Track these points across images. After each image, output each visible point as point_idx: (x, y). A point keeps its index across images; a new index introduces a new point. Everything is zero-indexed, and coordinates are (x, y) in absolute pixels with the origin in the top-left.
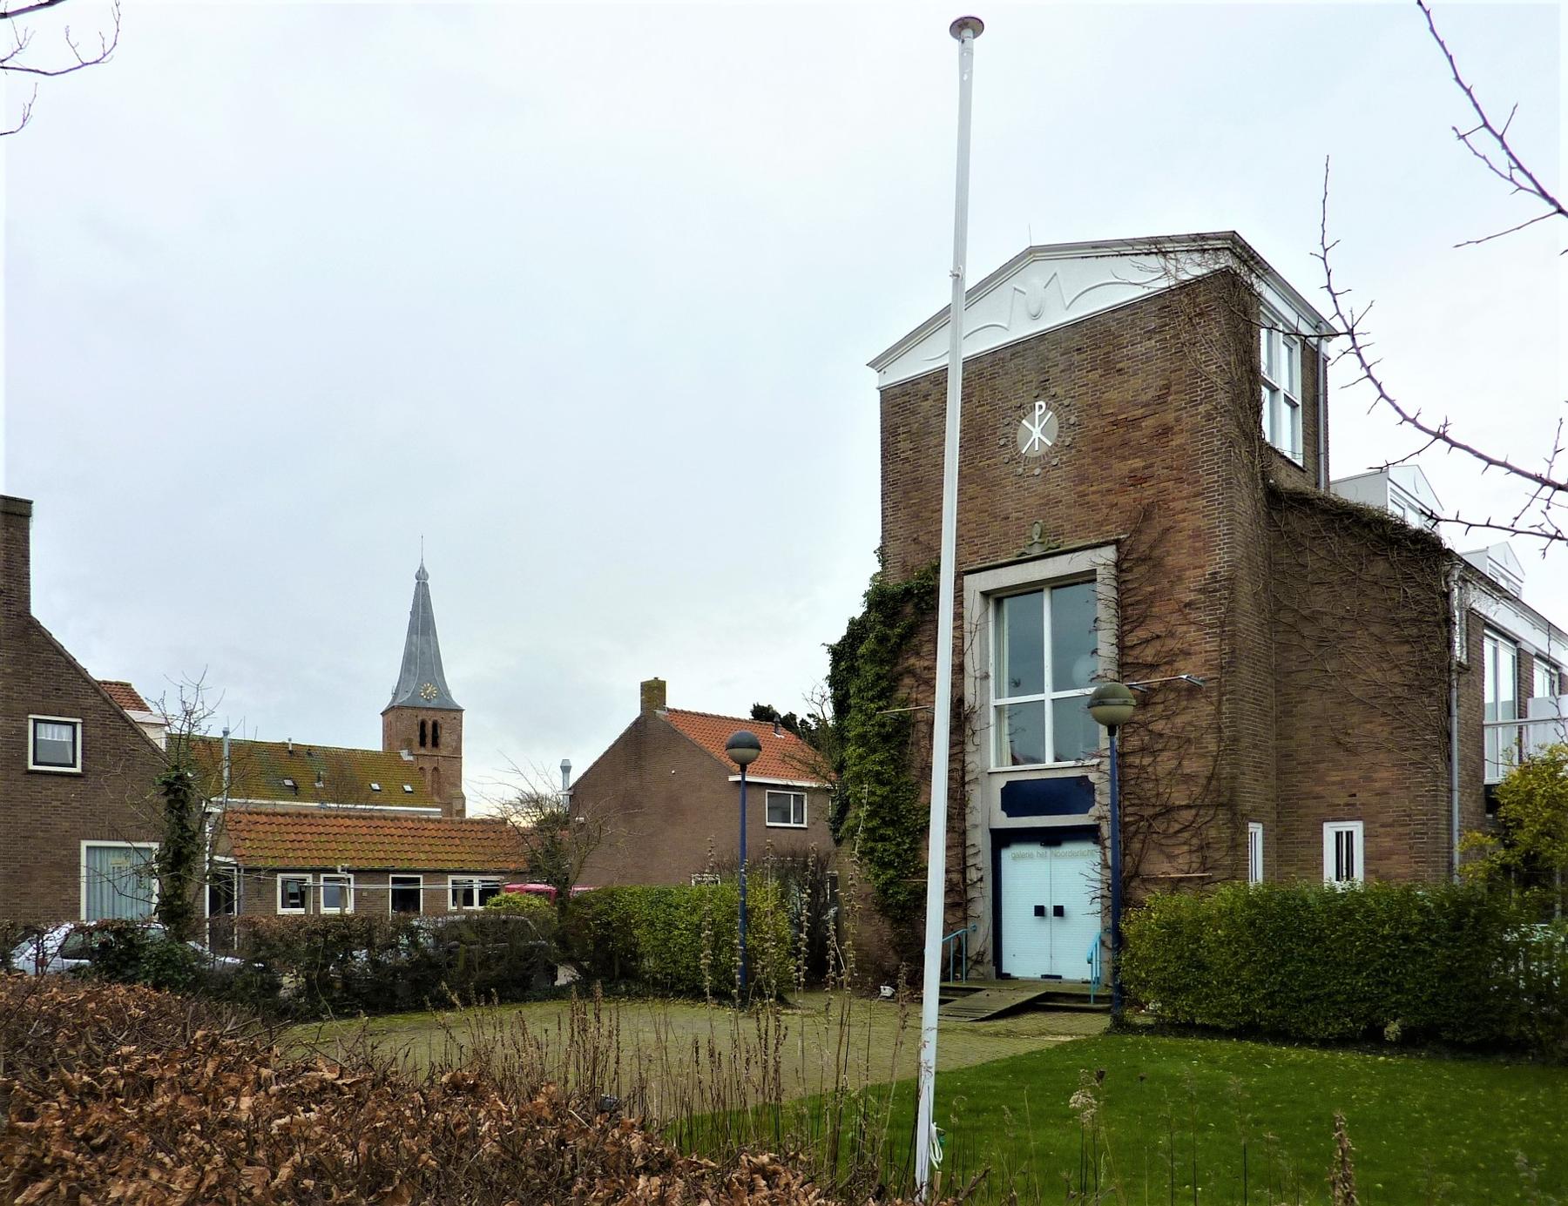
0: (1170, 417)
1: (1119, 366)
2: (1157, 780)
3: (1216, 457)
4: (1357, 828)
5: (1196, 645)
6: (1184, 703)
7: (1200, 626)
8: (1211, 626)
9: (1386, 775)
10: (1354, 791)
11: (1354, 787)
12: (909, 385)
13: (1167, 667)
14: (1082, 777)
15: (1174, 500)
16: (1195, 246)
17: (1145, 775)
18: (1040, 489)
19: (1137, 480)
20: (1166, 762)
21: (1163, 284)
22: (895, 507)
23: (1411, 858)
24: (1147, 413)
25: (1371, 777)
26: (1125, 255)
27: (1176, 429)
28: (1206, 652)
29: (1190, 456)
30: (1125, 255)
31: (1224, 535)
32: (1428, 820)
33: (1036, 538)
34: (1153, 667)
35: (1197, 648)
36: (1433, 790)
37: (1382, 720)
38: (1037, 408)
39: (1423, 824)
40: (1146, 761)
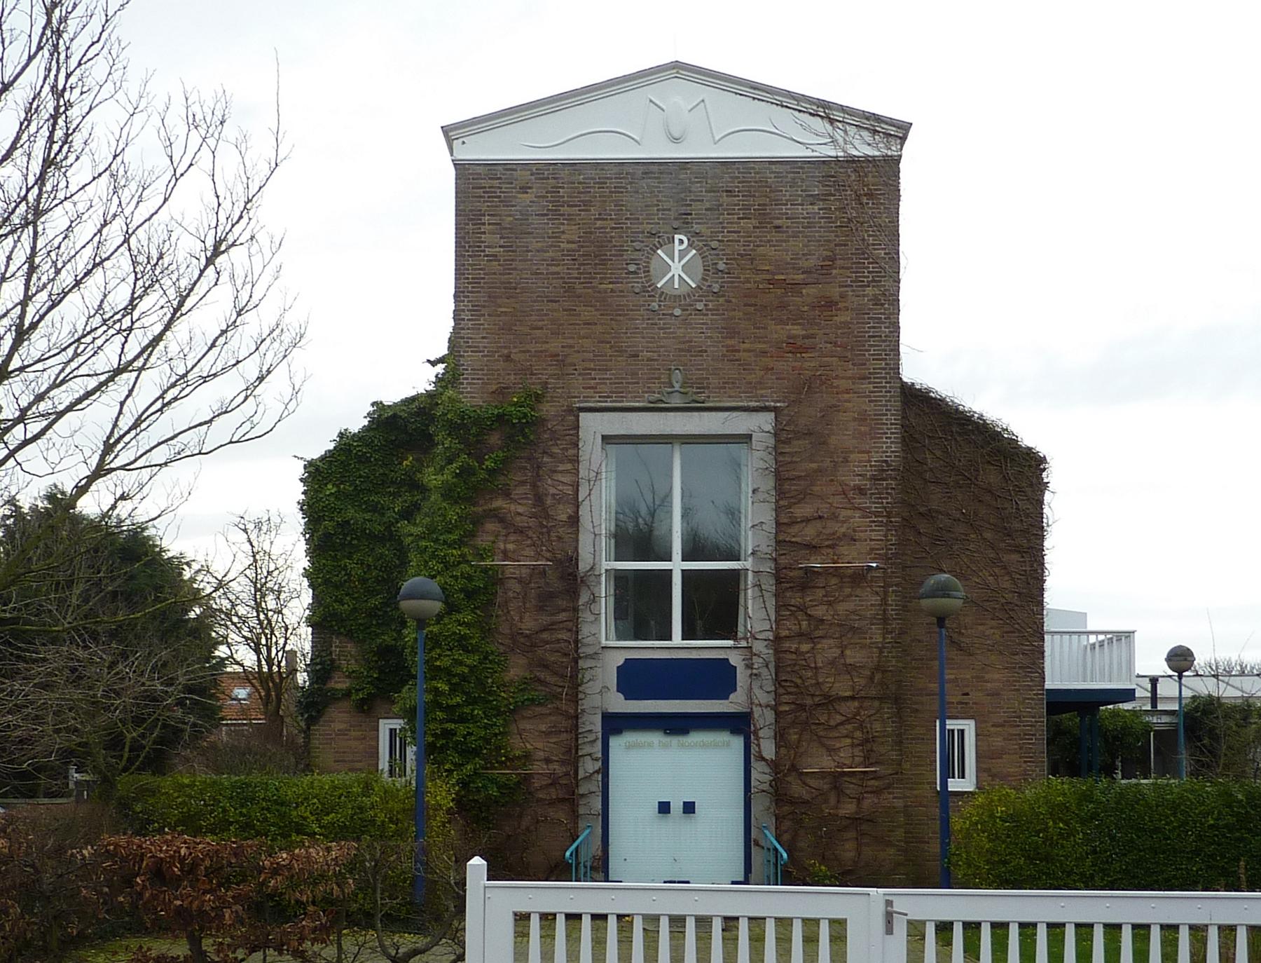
0: (835, 292)
1: (777, 222)
2: (816, 668)
3: (884, 344)
4: (969, 727)
5: (862, 531)
6: (847, 591)
7: (866, 513)
8: (877, 514)
9: (996, 676)
10: (966, 690)
11: (967, 686)
12: (500, 168)
13: (829, 550)
14: (724, 659)
15: (837, 377)
16: (867, 124)
17: (804, 663)
18: (680, 332)
19: (796, 348)
20: (827, 650)
21: (831, 152)
22: (476, 310)
23: (1020, 757)
24: (810, 280)
25: (983, 677)
26: (787, 107)
27: (840, 305)
28: (871, 540)
29: (856, 337)
30: (787, 107)
31: (891, 424)
32: (1036, 722)
33: (677, 386)
34: (813, 548)
35: (862, 534)
36: (1040, 694)
37: (994, 623)
38: (677, 242)
39: (1031, 726)
40: (805, 647)
